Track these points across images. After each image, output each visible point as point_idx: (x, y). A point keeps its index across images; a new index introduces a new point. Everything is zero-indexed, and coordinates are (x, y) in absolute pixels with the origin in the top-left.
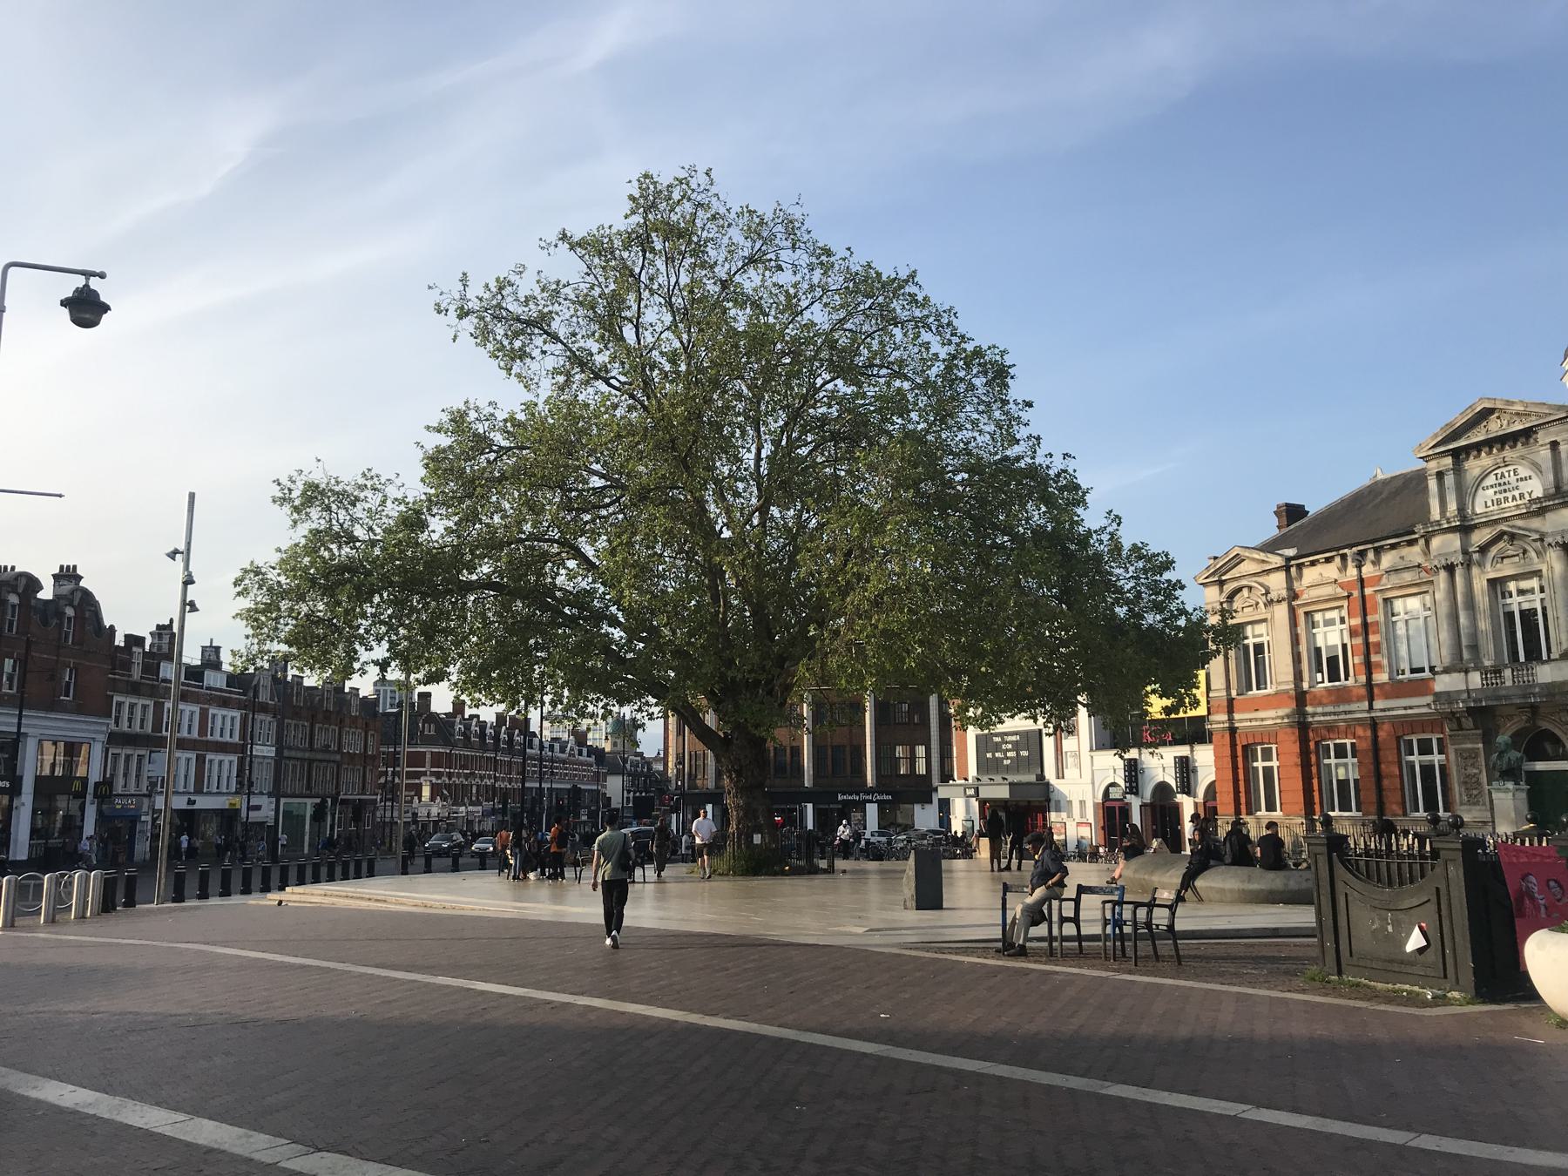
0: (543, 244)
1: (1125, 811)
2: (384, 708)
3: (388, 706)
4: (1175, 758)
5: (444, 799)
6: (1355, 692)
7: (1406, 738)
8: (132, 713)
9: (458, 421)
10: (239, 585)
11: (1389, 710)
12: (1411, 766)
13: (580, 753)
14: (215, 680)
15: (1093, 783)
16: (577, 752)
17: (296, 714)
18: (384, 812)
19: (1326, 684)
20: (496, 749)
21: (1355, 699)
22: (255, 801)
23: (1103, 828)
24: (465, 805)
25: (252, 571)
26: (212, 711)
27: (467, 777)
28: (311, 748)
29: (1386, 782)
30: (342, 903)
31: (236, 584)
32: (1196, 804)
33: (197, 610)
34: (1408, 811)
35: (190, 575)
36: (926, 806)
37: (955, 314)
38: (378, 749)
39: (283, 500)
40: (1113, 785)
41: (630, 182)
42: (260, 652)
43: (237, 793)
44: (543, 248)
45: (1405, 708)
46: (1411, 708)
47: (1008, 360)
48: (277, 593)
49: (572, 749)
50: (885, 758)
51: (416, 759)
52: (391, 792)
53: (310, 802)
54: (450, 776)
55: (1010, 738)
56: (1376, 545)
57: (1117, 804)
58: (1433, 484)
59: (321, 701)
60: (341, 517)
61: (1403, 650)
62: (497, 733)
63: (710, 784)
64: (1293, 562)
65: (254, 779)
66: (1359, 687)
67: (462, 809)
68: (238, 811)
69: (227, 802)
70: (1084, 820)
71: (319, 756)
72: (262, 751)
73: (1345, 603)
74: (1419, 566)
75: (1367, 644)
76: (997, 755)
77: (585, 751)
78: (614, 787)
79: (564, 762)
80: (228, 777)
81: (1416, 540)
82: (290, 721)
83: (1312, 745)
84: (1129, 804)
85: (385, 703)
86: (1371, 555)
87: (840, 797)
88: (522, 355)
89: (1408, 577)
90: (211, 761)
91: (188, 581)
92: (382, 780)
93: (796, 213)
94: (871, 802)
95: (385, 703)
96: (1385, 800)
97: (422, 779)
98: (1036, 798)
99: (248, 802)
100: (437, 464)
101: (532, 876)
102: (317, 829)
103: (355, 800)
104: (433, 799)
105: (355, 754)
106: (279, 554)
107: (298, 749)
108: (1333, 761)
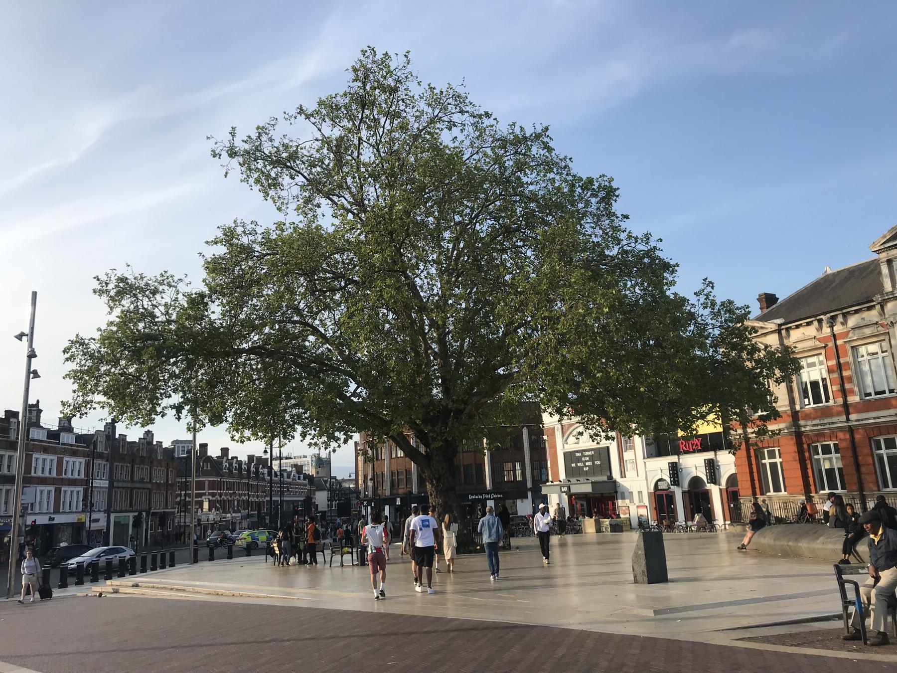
0: (287, 116)
1: (671, 498)
2: (178, 454)
3: (181, 452)
4: (705, 460)
5: (217, 509)
6: (835, 410)
7: (875, 438)
8: (10, 462)
9: (229, 236)
10: (68, 353)
11: (862, 420)
12: (881, 458)
13: (299, 478)
14: (68, 438)
15: (647, 480)
17: (122, 459)
18: (180, 519)
19: (812, 405)
20: (249, 477)
21: (834, 414)
22: (95, 516)
23: (656, 509)
24: (230, 513)
25: (78, 342)
26: (65, 459)
27: (231, 495)
28: (132, 481)
29: (863, 469)
30: (150, 593)
31: (65, 352)
32: (721, 490)
33: (39, 377)
34: (818, 489)
35: (33, 350)
36: (524, 500)
37: (570, 159)
38: (175, 480)
39: (101, 292)
40: (660, 480)
41: (347, 70)
42: (84, 402)
43: (83, 511)
44: (286, 119)
45: (874, 418)
46: (878, 418)
47: (614, 185)
48: (99, 359)
49: (294, 476)
50: (497, 472)
51: (200, 485)
52: (185, 507)
53: (131, 515)
54: (220, 495)
55: (587, 453)
56: (844, 311)
57: (664, 493)
58: (885, 269)
59: (138, 450)
60: (145, 303)
61: (868, 380)
62: (249, 467)
63: (386, 492)
64: (783, 327)
65: (94, 502)
66: (838, 406)
67: (229, 515)
68: (84, 523)
69: (76, 518)
70: (642, 504)
71: (137, 485)
72: (99, 483)
73: (823, 351)
74: (877, 323)
75: (842, 377)
76: (579, 464)
77: (302, 476)
78: (321, 499)
80: (77, 502)
81: (874, 306)
82: (118, 464)
83: (805, 446)
84: (673, 492)
85: (178, 451)
86: (840, 319)
87: (470, 497)
88: (275, 184)
89: (868, 331)
90: (65, 492)
91: (32, 355)
92: (178, 499)
93: (461, 90)
94: (490, 499)
95: (178, 451)
96: (864, 481)
97: (203, 497)
98: (607, 491)
99: (90, 517)
100: (214, 266)
101: (292, 560)
102: (136, 532)
103: (161, 513)
104: (210, 510)
105: (161, 483)
106: (100, 333)
107: (124, 481)
108: (821, 456)
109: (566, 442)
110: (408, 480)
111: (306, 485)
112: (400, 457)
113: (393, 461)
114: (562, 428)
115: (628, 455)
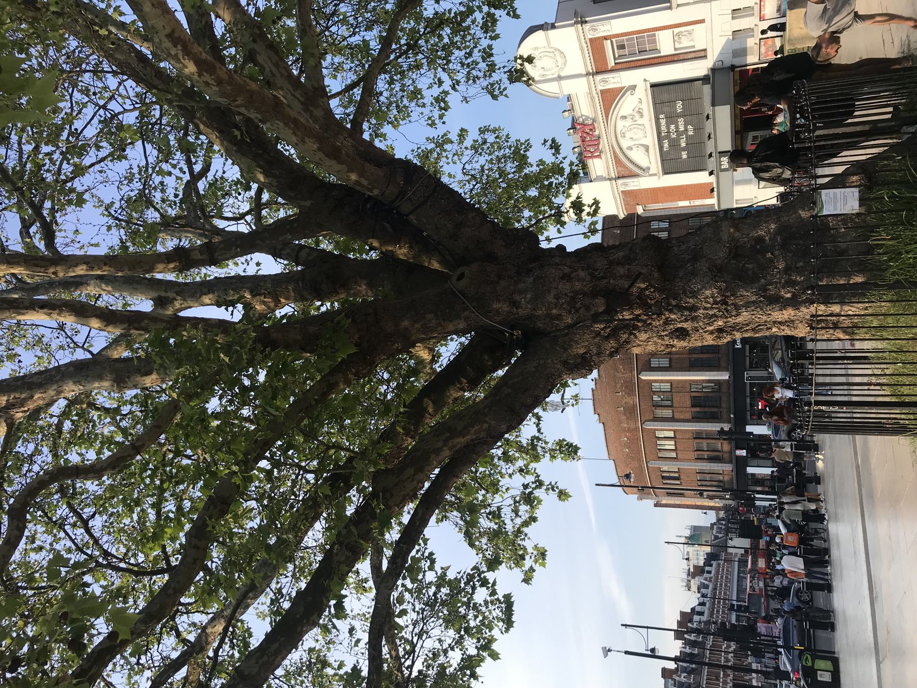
13: (709, 572)
16: (708, 575)
55: (664, 128)
63: (727, 469)
70: (757, 8)
77: (707, 568)
79: (715, 589)
98: (729, 86)
110: (708, 436)
111: (719, 565)
112: (675, 445)
114: (623, 177)
115: (666, 45)
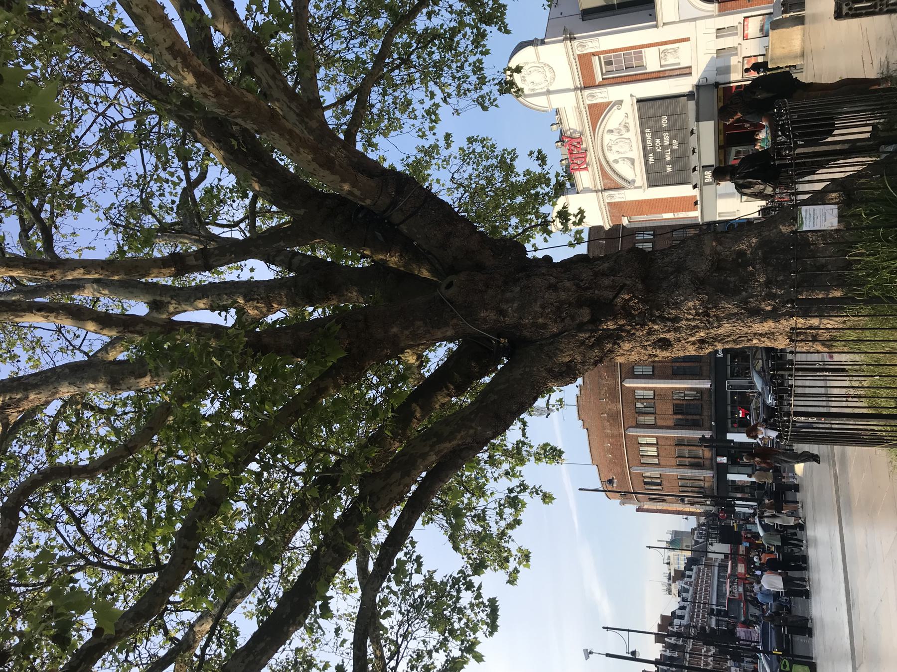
13: (690, 577)
15: (695, 19)
49: (686, 583)
55: (649, 142)
70: (740, 28)
77: (688, 573)
79: (695, 593)
109: (631, 182)
110: (690, 443)
111: (699, 569)
112: (658, 451)
113: (662, 463)
114: (609, 189)
